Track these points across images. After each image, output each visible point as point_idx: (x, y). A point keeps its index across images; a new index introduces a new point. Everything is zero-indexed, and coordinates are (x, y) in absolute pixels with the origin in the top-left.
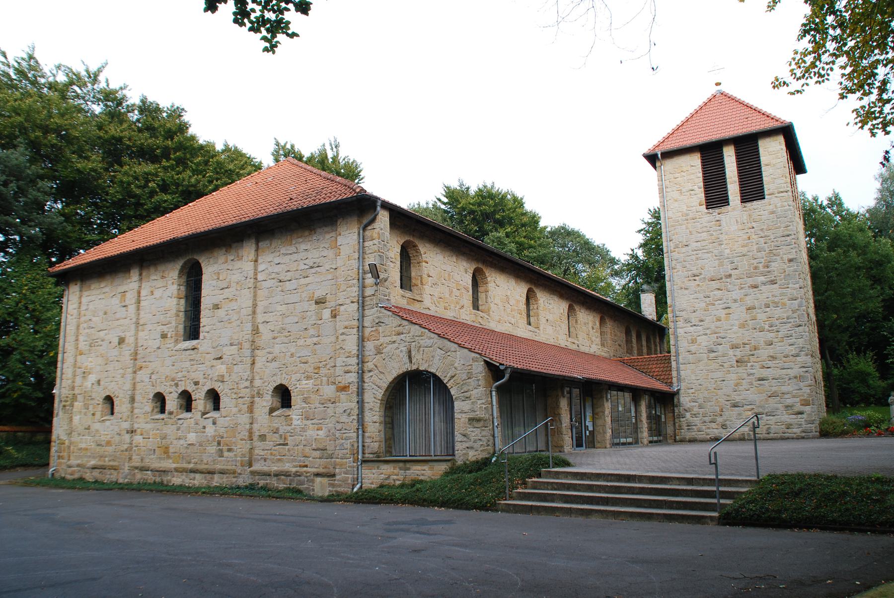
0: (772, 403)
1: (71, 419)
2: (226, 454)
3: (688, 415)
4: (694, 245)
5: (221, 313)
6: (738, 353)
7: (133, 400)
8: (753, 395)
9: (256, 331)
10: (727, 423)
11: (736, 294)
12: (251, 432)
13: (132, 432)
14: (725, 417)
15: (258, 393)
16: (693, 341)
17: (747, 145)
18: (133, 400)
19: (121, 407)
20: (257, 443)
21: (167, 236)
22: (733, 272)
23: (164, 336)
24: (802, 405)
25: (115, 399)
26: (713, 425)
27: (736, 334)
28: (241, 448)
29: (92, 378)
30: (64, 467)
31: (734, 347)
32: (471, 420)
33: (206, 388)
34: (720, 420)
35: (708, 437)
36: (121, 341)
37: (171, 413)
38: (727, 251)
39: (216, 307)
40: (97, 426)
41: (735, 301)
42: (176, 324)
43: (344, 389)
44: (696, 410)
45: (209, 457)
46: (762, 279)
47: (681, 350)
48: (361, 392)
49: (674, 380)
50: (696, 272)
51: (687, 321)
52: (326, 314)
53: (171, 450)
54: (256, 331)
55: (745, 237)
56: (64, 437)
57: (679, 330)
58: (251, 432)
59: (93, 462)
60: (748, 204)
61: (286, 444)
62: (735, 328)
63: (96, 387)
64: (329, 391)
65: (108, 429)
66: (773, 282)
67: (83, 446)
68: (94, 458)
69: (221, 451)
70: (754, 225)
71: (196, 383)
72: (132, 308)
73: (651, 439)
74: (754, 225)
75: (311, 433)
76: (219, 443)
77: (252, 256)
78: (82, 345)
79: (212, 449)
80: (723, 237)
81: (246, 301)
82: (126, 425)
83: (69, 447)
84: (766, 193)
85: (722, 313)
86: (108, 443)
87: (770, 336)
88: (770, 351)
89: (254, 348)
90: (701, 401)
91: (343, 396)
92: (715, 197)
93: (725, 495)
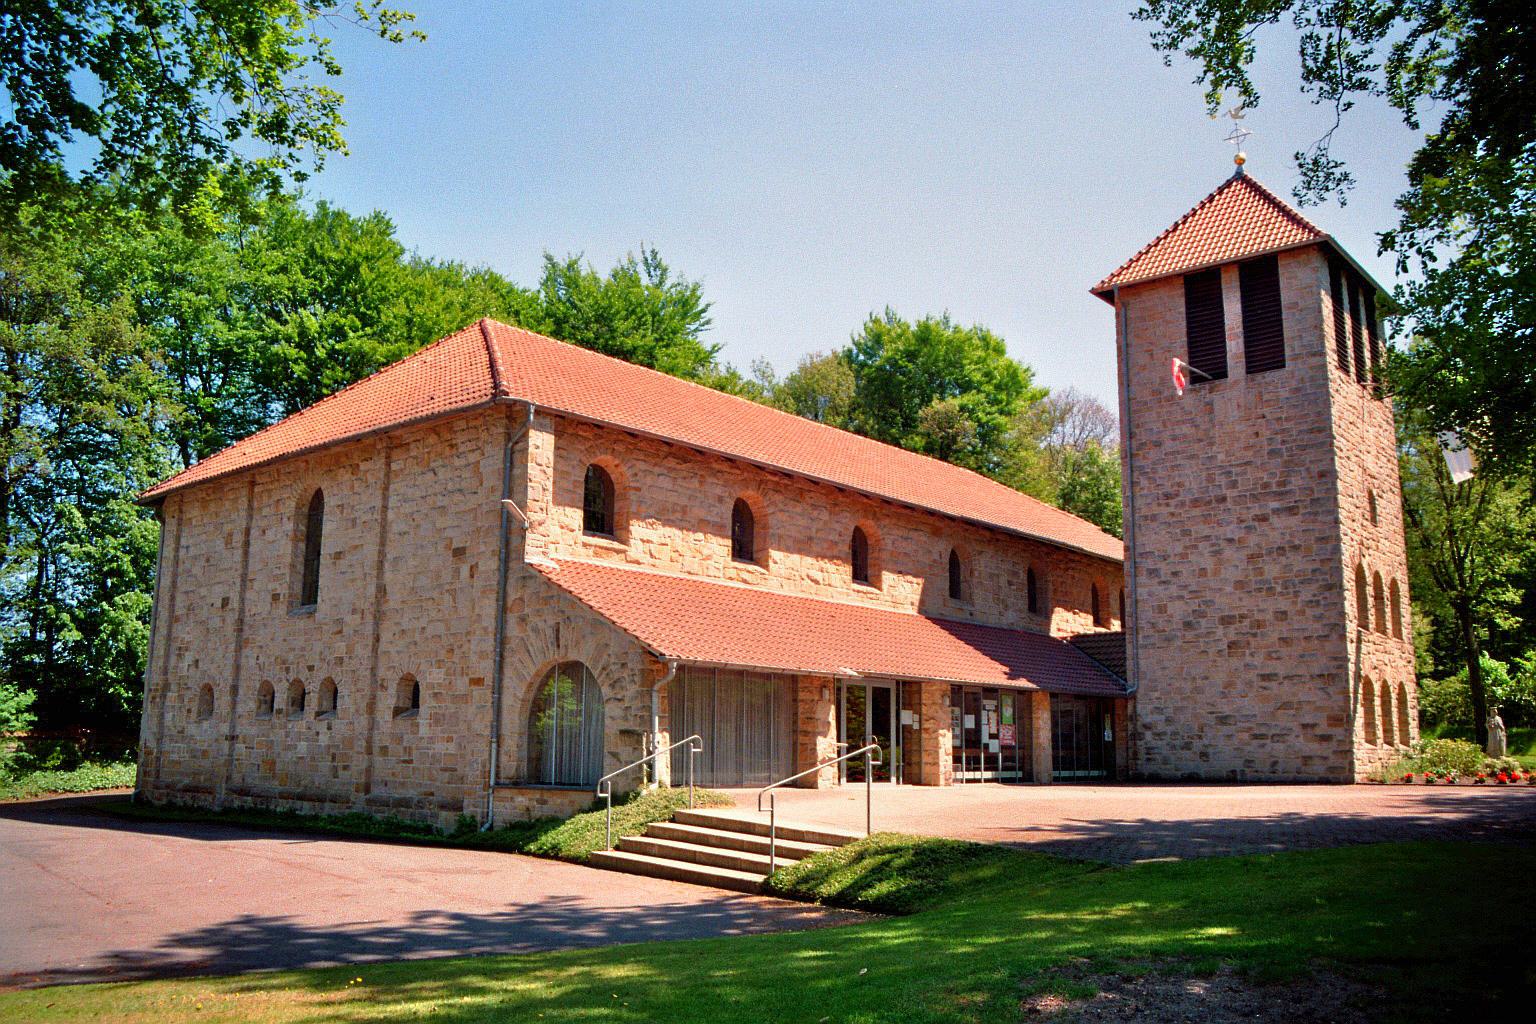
0: (1285, 720)
1: (162, 716)
2: (341, 772)
3: (1148, 735)
4: (1169, 445)
5: (343, 563)
6: (1232, 633)
7: (235, 690)
8: (1251, 705)
9: (382, 590)
10: (1210, 750)
11: (1232, 531)
12: (369, 742)
13: (233, 738)
14: (1206, 741)
15: (382, 686)
16: (1162, 609)
17: (1259, 274)
18: (235, 690)
19: (222, 702)
20: (378, 760)
21: (276, 450)
22: (1230, 493)
23: (276, 597)
24: (1330, 725)
25: (215, 689)
26: (1186, 754)
27: (1227, 601)
28: (359, 763)
29: (189, 657)
30: (150, 787)
31: (1226, 621)
32: (623, 732)
33: (323, 675)
34: (1197, 745)
35: (1179, 774)
36: (225, 602)
37: (280, 711)
38: (1221, 457)
39: (338, 555)
40: (192, 729)
41: (1230, 541)
42: (287, 583)
43: (478, 682)
44: (1161, 727)
45: (320, 777)
46: (1275, 505)
47: (1142, 623)
48: (498, 689)
49: (1129, 674)
50: (1169, 489)
51: (1153, 572)
52: (465, 571)
53: (279, 766)
54: (382, 590)
55: (1250, 431)
56: (152, 744)
57: (1139, 590)
58: (369, 742)
59: (186, 781)
60: (1259, 377)
61: (411, 762)
62: (1229, 589)
63: (192, 670)
64: (462, 685)
65: (205, 733)
66: (1291, 511)
67: (175, 757)
68: (187, 775)
69: (335, 769)
70: (1266, 411)
71: (311, 668)
72: (239, 553)
73: (1056, 774)
74: (1266, 411)
75: (440, 747)
76: (334, 758)
77: (243, 502)
78: (179, 612)
79: (325, 765)
80: (1216, 432)
81: (371, 551)
82: (225, 729)
83: (158, 759)
84: (1288, 352)
85: (1209, 563)
86: (205, 753)
87: (1283, 604)
88: (1282, 629)
89: (379, 617)
90: (1170, 712)
91: (477, 691)
92: (1207, 363)
93: (783, 853)
